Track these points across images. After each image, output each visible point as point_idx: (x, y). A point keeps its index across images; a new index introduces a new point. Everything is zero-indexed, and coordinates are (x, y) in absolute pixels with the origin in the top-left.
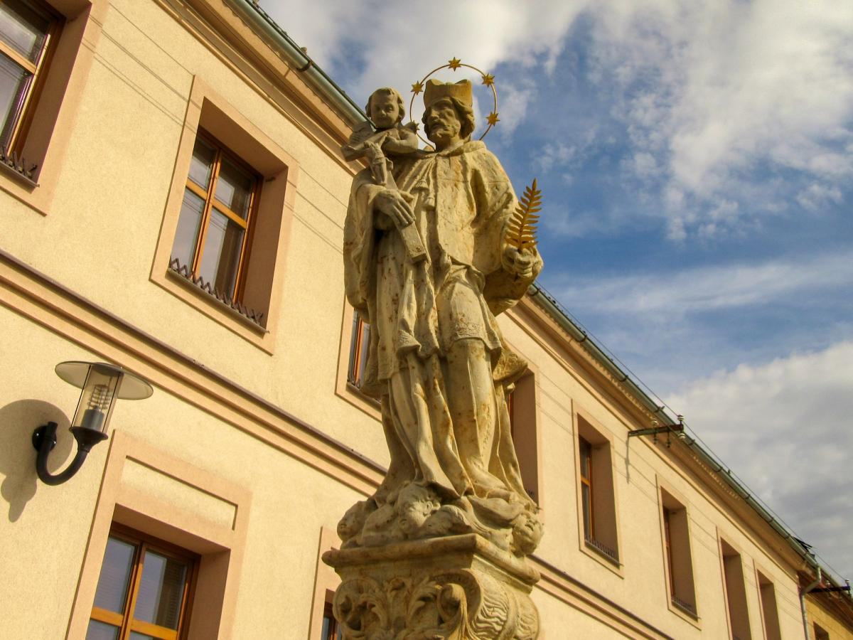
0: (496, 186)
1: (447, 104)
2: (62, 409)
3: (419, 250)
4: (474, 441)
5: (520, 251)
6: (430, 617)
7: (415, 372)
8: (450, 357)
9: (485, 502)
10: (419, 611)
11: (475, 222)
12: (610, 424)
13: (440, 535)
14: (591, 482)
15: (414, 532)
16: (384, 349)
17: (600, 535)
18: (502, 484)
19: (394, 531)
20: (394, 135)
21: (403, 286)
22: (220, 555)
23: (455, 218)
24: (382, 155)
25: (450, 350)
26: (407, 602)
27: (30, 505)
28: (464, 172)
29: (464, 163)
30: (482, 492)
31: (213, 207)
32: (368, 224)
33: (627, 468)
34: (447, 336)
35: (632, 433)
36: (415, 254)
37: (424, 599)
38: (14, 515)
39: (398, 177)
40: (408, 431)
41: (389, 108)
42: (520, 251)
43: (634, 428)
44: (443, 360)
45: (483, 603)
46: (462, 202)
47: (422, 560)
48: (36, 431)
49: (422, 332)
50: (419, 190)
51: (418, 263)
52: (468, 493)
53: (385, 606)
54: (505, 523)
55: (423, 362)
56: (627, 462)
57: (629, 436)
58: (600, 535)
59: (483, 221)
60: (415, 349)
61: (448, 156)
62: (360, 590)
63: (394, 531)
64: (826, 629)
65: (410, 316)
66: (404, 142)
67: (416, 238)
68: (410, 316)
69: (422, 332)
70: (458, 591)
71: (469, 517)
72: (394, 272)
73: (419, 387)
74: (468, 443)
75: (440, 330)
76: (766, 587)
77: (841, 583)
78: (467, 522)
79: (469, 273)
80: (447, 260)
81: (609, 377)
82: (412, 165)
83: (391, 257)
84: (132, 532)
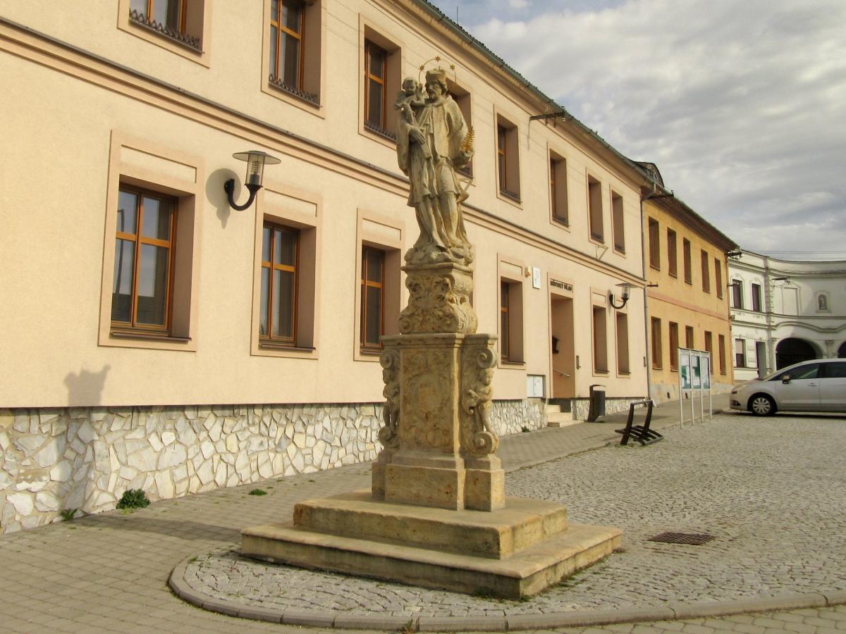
0: (456, 119)
1: (436, 83)
2: (229, 168)
3: (428, 154)
4: (451, 227)
5: (466, 152)
6: (439, 288)
7: (429, 204)
8: (442, 197)
9: (455, 249)
10: (435, 286)
11: (449, 135)
12: (517, 114)
13: (440, 262)
14: (505, 153)
15: (432, 261)
16: (416, 191)
17: (509, 187)
18: (461, 241)
19: (426, 261)
20: (414, 98)
21: (423, 168)
22: (310, 230)
23: (441, 135)
24: (411, 110)
25: (442, 195)
26: (431, 283)
27: (230, 220)
28: (444, 114)
29: (443, 109)
30: (454, 245)
31: (282, 31)
32: (407, 142)
33: (528, 141)
34: (440, 190)
35: (532, 118)
36: (427, 156)
37: (437, 282)
38: (224, 225)
39: (417, 116)
40: (427, 223)
41: (412, 87)
42: (466, 152)
43: (534, 115)
44: (439, 198)
45: (456, 284)
46: (443, 127)
47: (436, 270)
48: (225, 185)
49: (431, 188)
50: (426, 125)
51: (428, 159)
52: (450, 247)
53: (424, 284)
54: (462, 257)
55: (432, 199)
56: (528, 137)
57: (530, 120)
58: (509, 187)
59: (452, 135)
60: (429, 195)
61: (437, 106)
62: (414, 279)
63: (426, 261)
64: (657, 219)
65: (426, 181)
66: (419, 102)
67: (427, 149)
68: (426, 181)
69: (431, 188)
70: (448, 280)
71: (451, 256)
72: (418, 161)
73: (431, 209)
74: (448, 227)
75: (437, 186)
76: (617, 199)
77: (670, 192)
78: (450, 258)
79: (447, 160)
80: (439, 157)
81: (518, 85)
82: (422, 110)
83: (417, 153)
84: (271, 224)
